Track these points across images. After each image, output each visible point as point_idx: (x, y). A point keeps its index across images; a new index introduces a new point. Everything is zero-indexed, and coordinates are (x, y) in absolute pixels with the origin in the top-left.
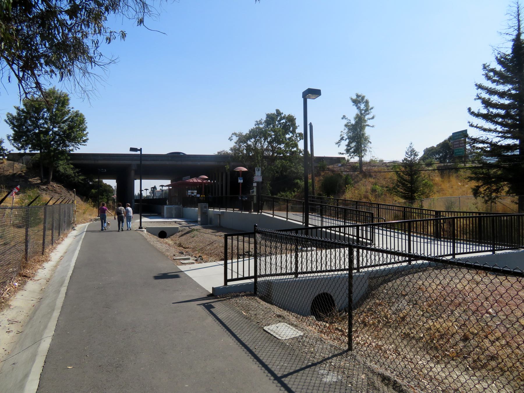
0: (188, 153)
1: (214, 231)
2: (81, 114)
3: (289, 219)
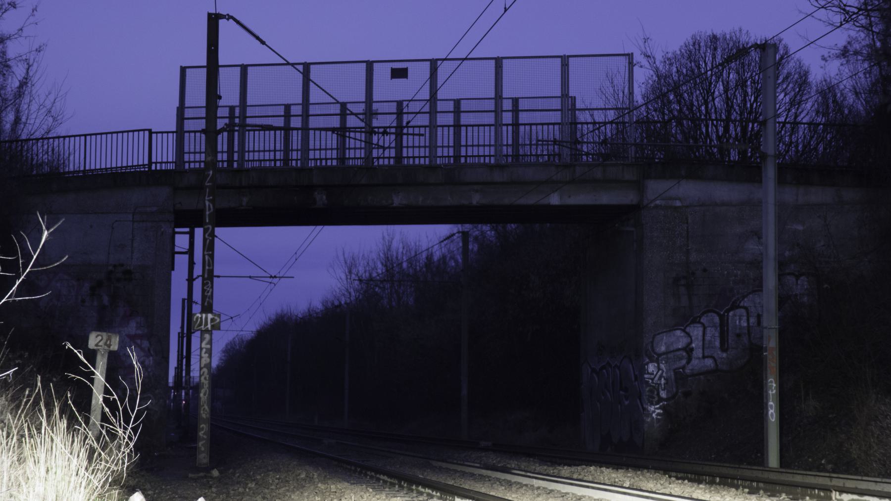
0: (261, 38)
2: (217, 366)
3: (249, 134)
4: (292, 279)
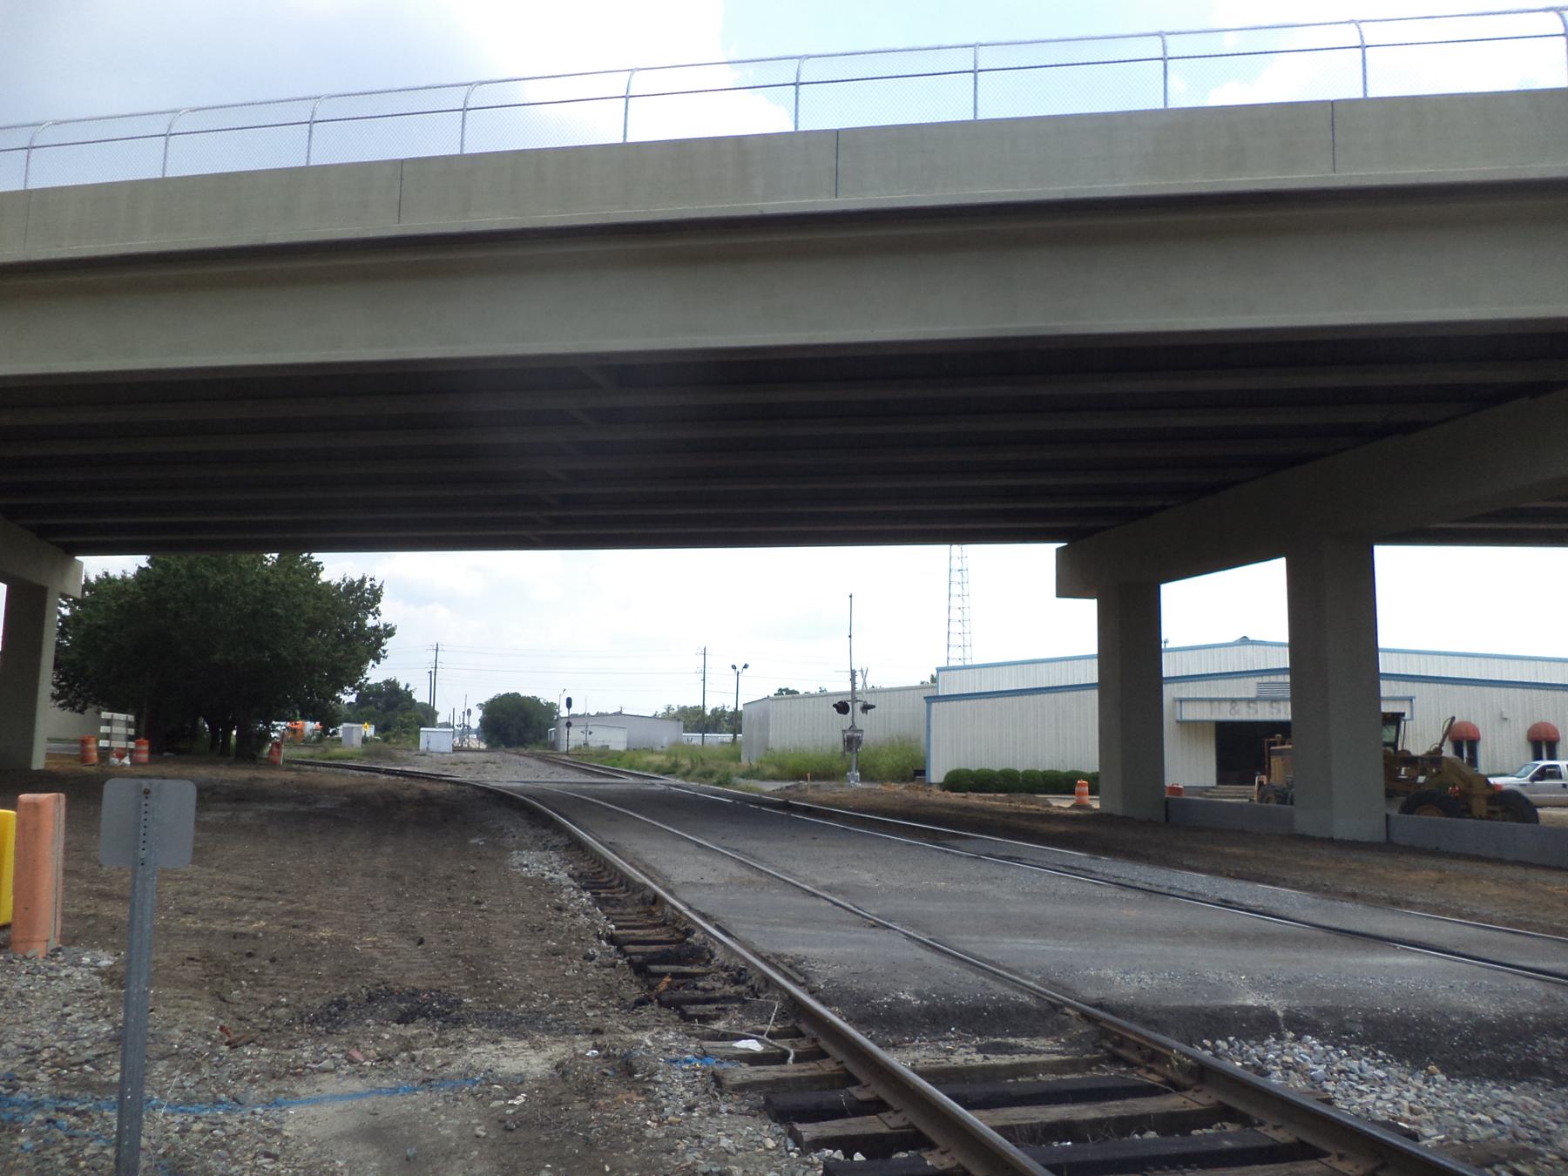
1: (1093, 856)
2: (552, 703)
4: (53, 736)
